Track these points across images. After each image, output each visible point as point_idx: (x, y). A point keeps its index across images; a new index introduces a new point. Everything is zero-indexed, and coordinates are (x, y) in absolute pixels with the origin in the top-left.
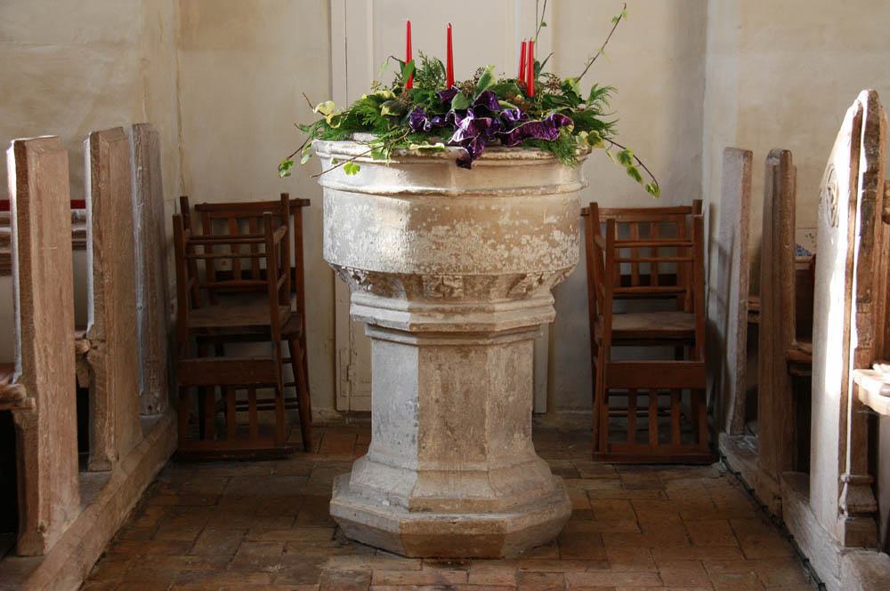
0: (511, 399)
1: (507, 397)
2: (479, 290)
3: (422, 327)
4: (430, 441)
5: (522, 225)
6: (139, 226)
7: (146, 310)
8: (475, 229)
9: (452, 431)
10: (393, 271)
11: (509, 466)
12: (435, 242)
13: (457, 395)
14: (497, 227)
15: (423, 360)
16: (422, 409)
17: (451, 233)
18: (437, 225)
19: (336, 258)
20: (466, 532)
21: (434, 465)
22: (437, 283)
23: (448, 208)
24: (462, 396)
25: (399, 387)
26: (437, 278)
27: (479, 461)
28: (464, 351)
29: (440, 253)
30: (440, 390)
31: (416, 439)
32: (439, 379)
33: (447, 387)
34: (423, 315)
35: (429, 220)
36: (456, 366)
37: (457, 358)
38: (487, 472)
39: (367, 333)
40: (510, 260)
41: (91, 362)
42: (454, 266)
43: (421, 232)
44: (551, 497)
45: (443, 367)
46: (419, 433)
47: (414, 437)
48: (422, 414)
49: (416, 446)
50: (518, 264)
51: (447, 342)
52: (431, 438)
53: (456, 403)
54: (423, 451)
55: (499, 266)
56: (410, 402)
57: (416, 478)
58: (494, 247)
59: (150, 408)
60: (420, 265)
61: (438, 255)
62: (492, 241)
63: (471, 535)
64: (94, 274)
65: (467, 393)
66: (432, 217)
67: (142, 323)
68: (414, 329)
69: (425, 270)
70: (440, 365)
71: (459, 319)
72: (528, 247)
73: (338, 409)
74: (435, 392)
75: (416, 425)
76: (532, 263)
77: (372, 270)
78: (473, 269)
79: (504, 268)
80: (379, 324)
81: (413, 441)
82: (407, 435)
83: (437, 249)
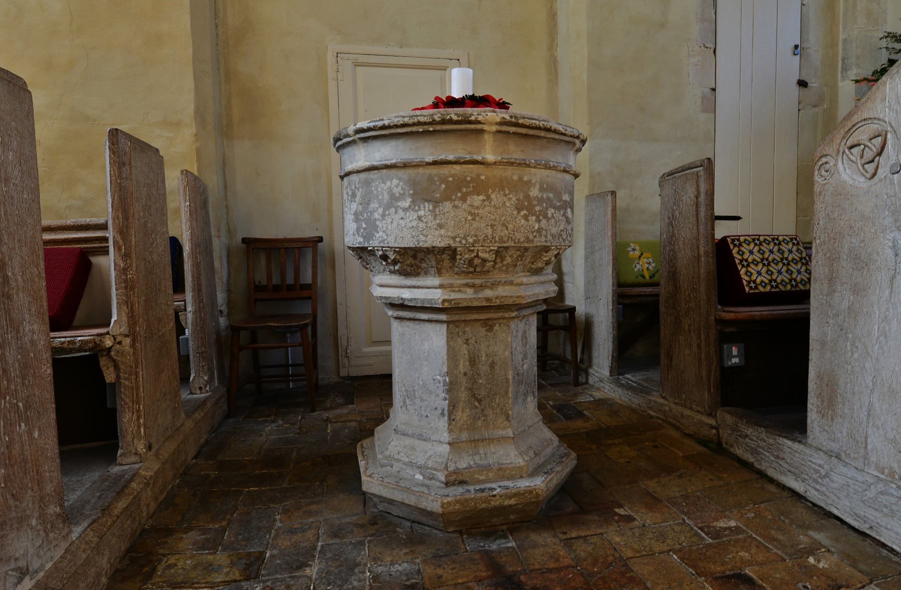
0: (525, 366)
1: (523, 365)
2: (508, 264)
3: (453, 302)
4: (460, 413)
5: (548, 198)
6: (187, 248)
7: (195, 312)
8: (510, 199)
9: (480, 401)
10: (426, 245)
11: (527, 428)
12: (470, 213)
13: (484, 368)
14: (528, 197)
15: (450, 337)
16: (451, 383)
17: (486, 203)
18: (473, 195)
19: (362, 240)
20: (506, 503)
21: (464, 436)
22: (473, 255)
23: (483, 177)
24: (488, 369)
25: (425, 363)
26: (473, 251)
27: (505, 428)
28: (488, 325)
29: (475, 224)
30: (468, 363)
31: (446, 412)
32: (466, 353)
33: (474, 361)
34: (454, 291)
35: (464, 190)
36: (482, 339)
37: (483, 331)
38: (513, 438)
39: (390, 313)
40: (539, 230)
41: (115, 357)
42: (490, 237)
43: (456, 202)
44: (557, 450)
45: (470, 341)
46: (449, 406)
47: (443, 410)
48: (451, 388)
49: (446, 418)
50: (546, 236)
51: (475, 316)
52: (460, 409)
53: (482, 375)
54: (454, 422)
55: (531, 237)
56: (438, 377)
57: (448, 450)
58: (526, 218)
59: (200, 388)
60: (456, 237)
61: (475, 226)
62: (525, 212)
63: (510, 506)
64: (115, 269)
65: (492, 366)
66: (467, 187)
67: (192, 324)
68: (446, 305)
69: (460, 242)
70: (467, 340)
71: (488, 293)
72: (553, 221)
73: (341, 376)
74: (463, 365)
75: (445, 399)
76: (555, 236)
77: (402, 246)
78: (508, 240)
79: (535, 239)
80: (406, 303)
81: (443, 414)
82: (436, 409)
83: (473, 219)
